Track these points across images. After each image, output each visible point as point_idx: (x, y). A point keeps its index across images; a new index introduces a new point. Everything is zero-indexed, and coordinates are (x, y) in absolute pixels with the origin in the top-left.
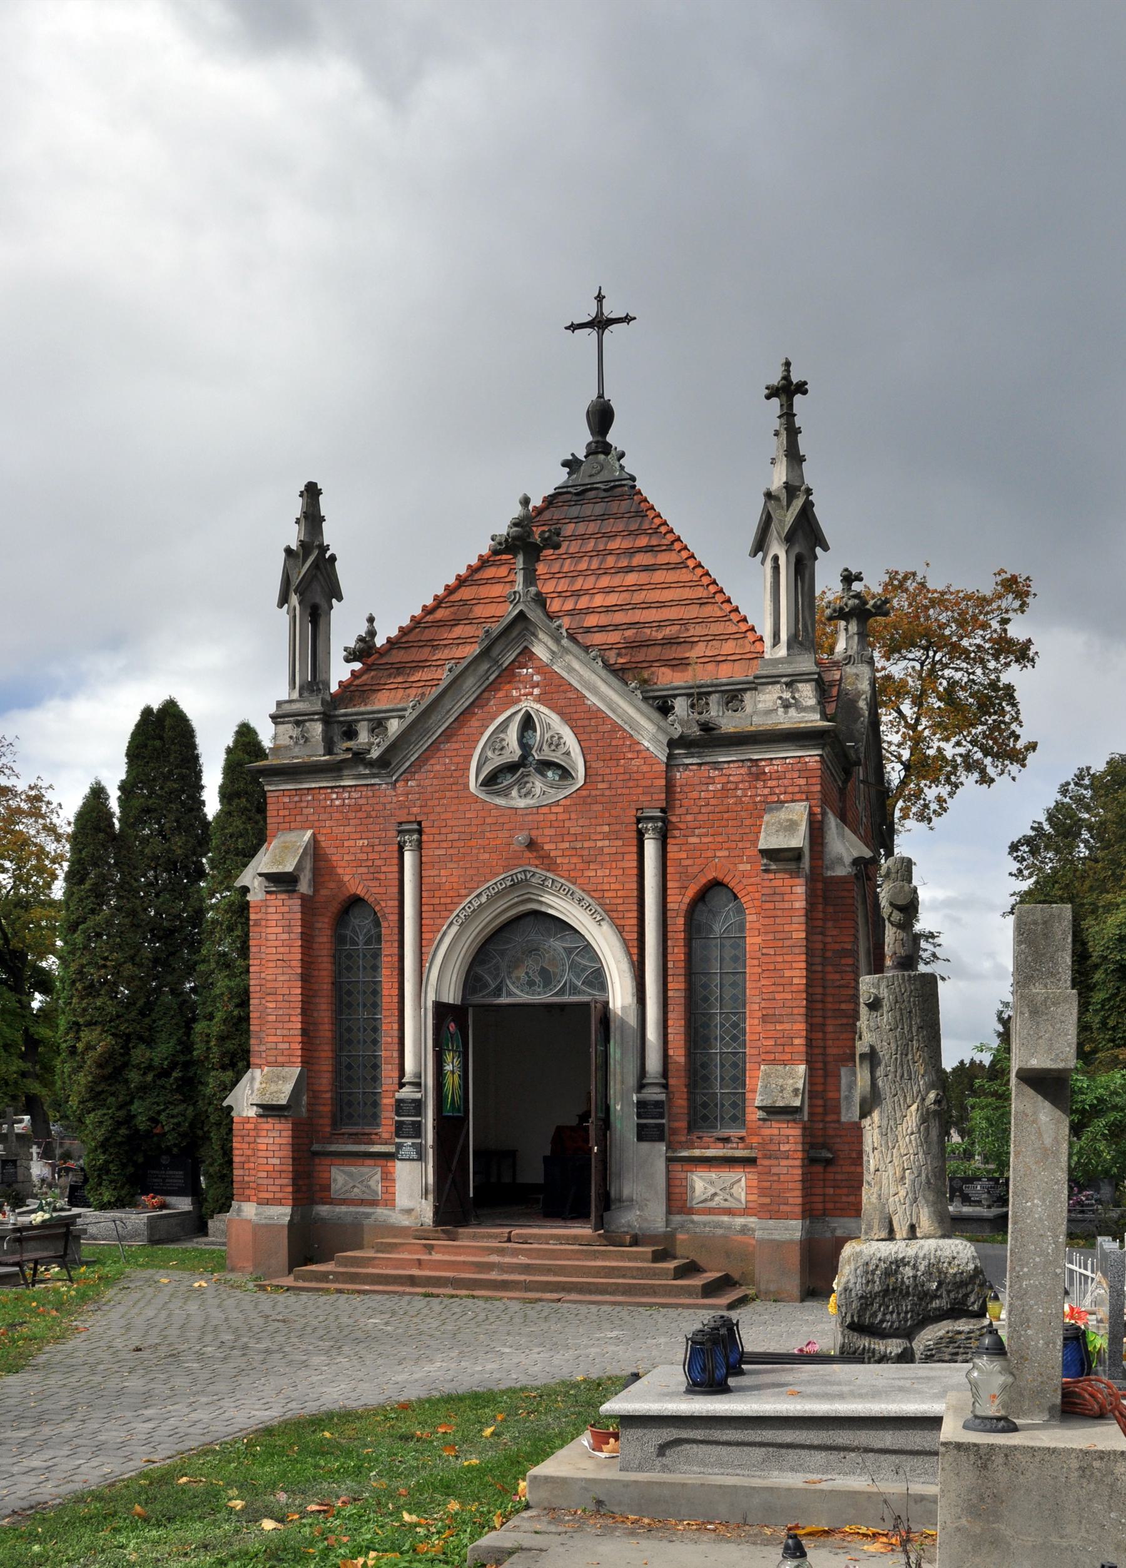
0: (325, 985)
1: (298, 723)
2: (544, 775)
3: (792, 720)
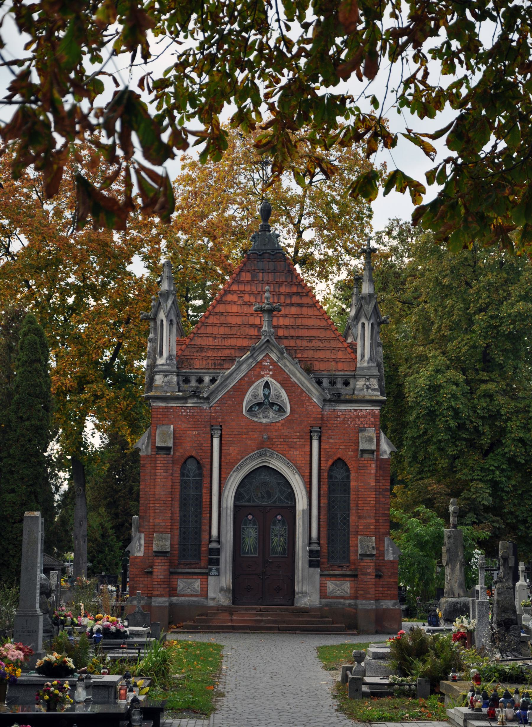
3: (369, 394)
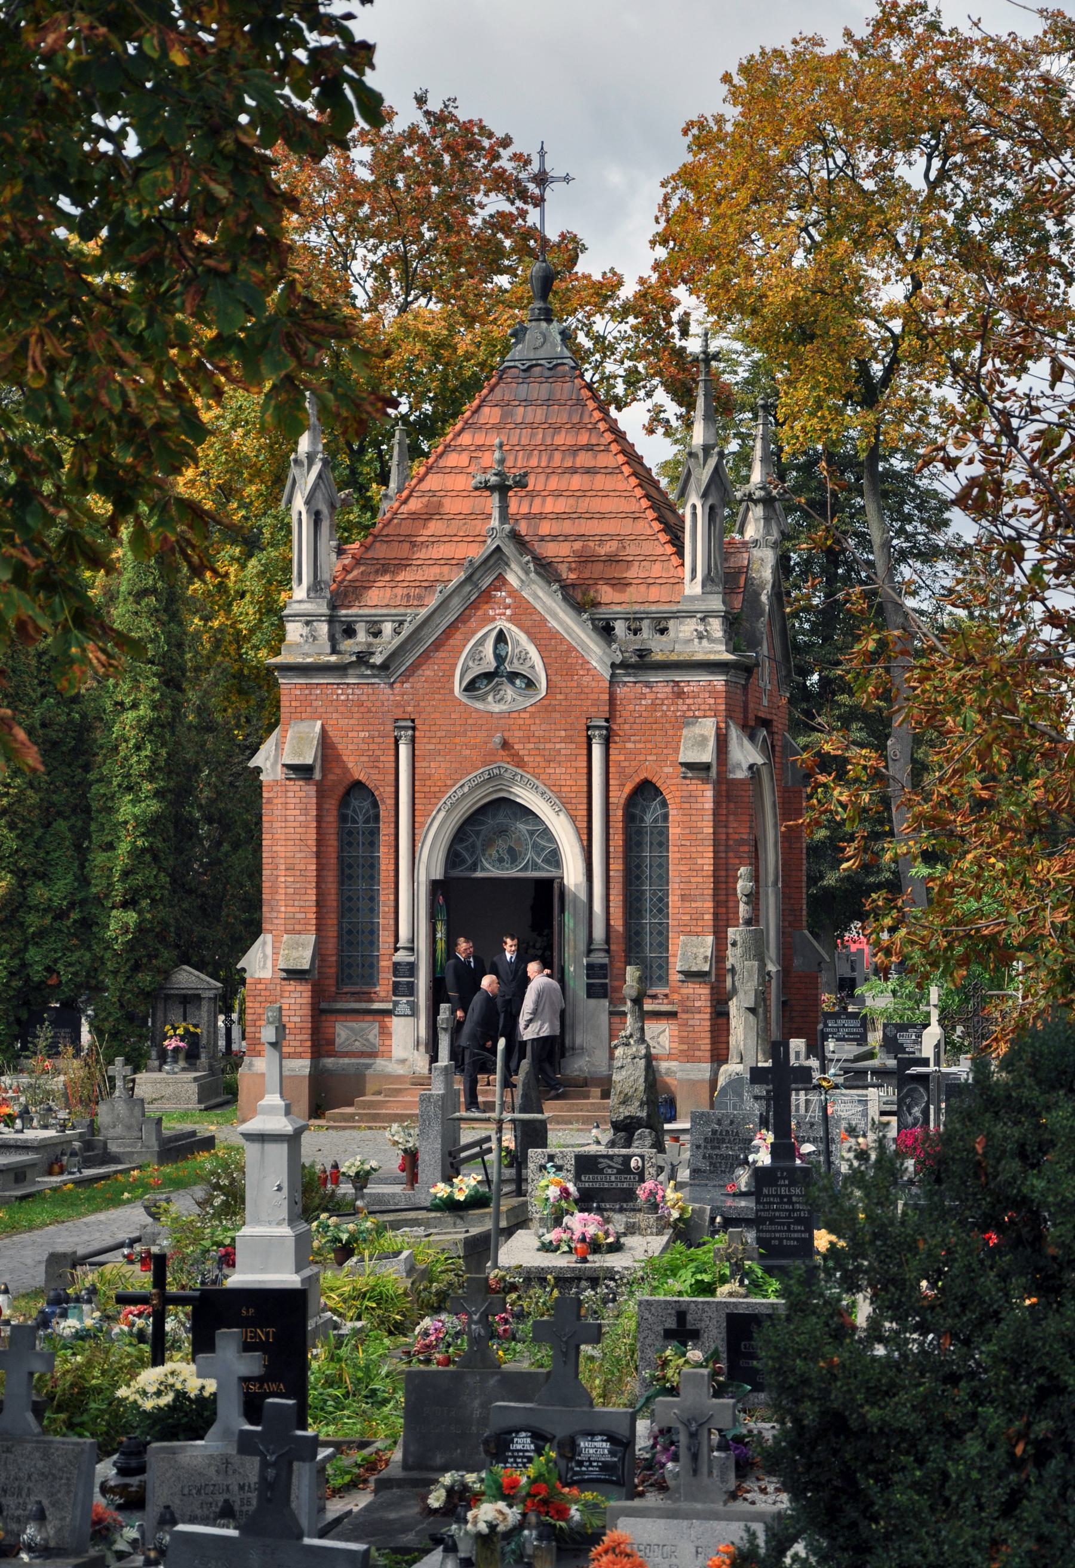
0: (332, 861)
1: (307, 623)
2: (513, 684)
